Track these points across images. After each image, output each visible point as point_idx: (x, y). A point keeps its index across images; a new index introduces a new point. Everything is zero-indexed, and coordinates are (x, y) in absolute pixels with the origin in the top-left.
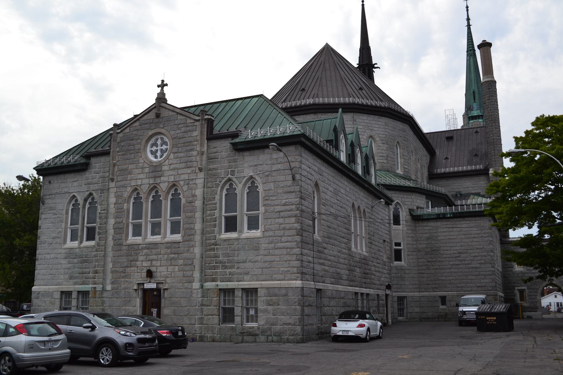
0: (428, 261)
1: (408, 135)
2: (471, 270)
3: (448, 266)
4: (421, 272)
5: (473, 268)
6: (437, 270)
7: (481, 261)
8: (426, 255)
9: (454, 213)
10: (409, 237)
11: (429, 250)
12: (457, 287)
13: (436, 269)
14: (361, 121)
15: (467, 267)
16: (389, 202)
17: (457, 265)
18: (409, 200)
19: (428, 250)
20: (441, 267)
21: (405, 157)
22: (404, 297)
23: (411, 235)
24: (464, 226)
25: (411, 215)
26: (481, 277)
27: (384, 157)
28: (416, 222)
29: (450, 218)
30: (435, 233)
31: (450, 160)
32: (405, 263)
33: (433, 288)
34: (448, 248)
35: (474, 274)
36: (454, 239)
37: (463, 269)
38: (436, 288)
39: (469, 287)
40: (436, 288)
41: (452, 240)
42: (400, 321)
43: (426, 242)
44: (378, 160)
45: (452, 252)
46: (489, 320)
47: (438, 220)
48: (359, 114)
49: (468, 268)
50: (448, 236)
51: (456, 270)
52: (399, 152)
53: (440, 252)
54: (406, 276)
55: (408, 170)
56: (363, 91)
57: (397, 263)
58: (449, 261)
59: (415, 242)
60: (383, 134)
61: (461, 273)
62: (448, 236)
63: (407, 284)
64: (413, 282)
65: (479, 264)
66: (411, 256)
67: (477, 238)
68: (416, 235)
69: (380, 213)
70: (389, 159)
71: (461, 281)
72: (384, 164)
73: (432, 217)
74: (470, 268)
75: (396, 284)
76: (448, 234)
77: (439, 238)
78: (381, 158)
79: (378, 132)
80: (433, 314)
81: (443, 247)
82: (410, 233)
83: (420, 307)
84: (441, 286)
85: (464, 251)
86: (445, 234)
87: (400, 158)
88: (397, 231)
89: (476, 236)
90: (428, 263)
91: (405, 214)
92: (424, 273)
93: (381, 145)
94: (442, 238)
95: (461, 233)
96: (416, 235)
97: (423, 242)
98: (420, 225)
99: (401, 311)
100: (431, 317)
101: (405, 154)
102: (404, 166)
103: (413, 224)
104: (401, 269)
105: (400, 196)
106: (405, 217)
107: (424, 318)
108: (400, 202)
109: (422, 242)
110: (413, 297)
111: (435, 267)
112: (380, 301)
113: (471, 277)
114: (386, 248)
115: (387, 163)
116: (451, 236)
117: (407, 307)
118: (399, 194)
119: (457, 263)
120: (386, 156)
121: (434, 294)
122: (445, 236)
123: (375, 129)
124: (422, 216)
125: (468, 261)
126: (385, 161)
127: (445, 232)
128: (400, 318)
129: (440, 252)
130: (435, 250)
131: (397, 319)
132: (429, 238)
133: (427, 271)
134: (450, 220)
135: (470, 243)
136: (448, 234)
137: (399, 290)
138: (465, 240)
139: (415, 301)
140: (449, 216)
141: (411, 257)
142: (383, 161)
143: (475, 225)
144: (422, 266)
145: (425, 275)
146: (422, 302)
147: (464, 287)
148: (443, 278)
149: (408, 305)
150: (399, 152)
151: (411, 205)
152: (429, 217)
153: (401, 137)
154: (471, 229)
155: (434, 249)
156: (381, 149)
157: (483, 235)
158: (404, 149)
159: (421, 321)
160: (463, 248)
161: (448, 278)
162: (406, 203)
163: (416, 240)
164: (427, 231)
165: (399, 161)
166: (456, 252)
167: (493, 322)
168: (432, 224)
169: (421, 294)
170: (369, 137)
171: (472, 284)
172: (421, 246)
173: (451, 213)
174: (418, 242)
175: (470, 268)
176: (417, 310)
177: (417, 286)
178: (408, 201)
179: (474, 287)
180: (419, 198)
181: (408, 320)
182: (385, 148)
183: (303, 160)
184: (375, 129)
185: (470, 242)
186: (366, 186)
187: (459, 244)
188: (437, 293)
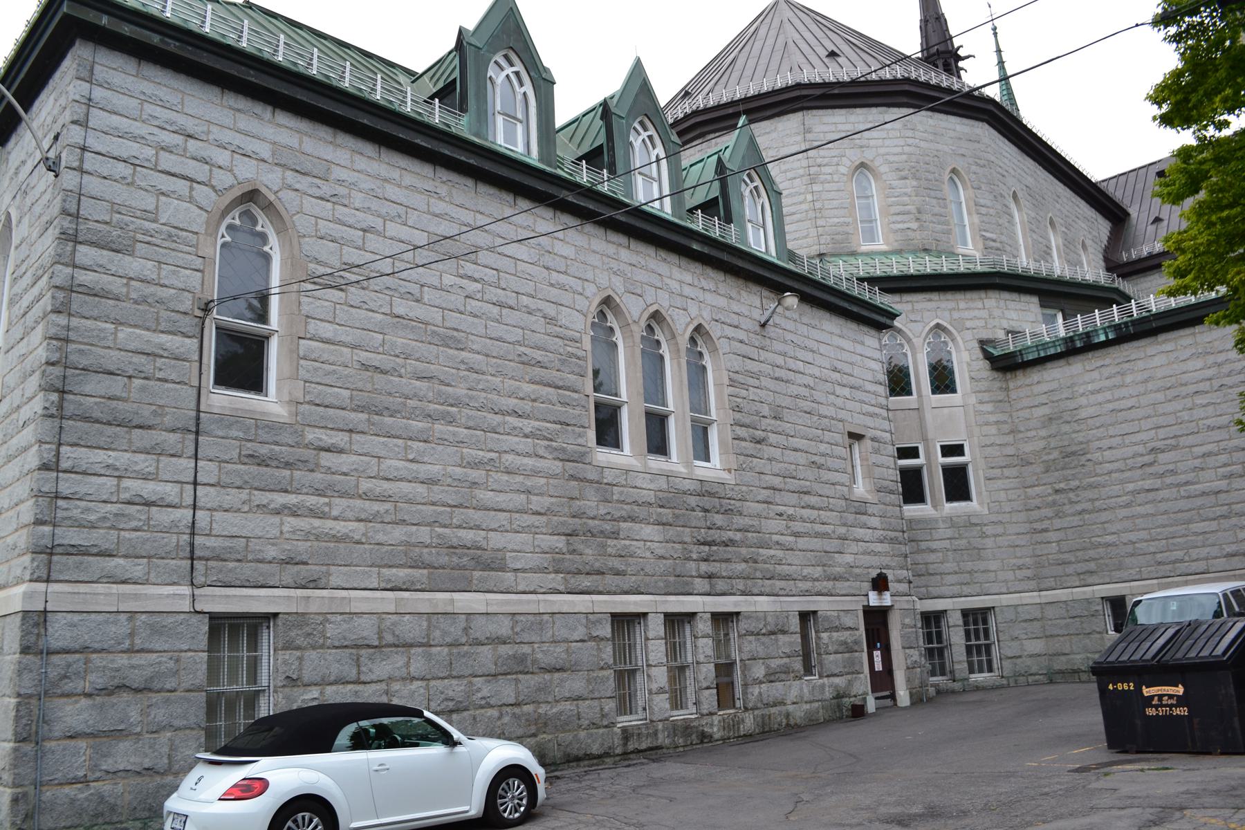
0: (1057, 491)
1: (989, 149)
2: (1199, 502)
3: (1119, 500)
4: (1038, 526)
5: (1203, 494)
6: (1087, 516)
7: (1229, 469)
8: (1047, 471)
9: (1117, 327)
10: (987, 424)
11: (1055, 454)
12: (1159, 563)
13: (1084, 511)
14: (826, 128)
15: (1183, 493)
16: (879, 321)
17: (1148, 491)
18: (976, 313)
19: (1051, 457)
20: (1097, 504)
21: (983, 210)
22: (989, 609)
23: (992, 418)
24: (1157, 361)
25: (988, 356)
26: (1234, 520)
27: (909, 213)
28: (1009, 375)
29: (1107, 344)
30: (1067, 399)
31: (1165, 223)
32: (981, 503)
33: (1079, 574)
34: (1112, 439)
35: (1211, 515)
36: (1130, 409)
37: (1170, 503)
38: (1091, 573)
39: (1197, 560)
40: (1091, 573)
41: (1123, 413)
42: (978, 688)
43: (1043, 433)
44: (892, 226)
45: (1129, 451)
46: (1155, 702)
47: (1071, 359)
48: (821, 112)
49: (1188, 497)
50: (1109, 401)
51: (1149, 509)
52: (963, 199)
53: (1089, 456)
54: (989, 542)
55: (998, 245)
56: (839, 60)
57: (951, 508)
58: (1123, 482)
59: (1010, 439)
60: (901, 154)
61: (1165, 517)
62: (1109, 401)
63: (993, 569)
64: (1014, 561)
65: (1225, 477)
66: (1000, 482)
67: (1207, 392)
68: (1011, 416)
69: (823, 349)
70: (925, 217)
71: (1171, 541)
72: (910, 233)
73: (1052, 351)
74: (1196, 496)
75: (956, 573)
76: (1108, 395)
77: (1083, 414)
78: (899, 218)
79: (882, 151)
80: (1088, 658)
81: (1099, 439)
82: (989, 413)
83: (1047, 637)
84: (1107, 565)
85: (1169, 442)
86: (1100, 397)
87: (969, 213)
88: (946, 411)
89: (1201, 387)
90: (1057, 497)
91: (966, 356)
92: (1045, 530)
93: (895, 183)
94: (1091, 411)
95: (1150, 386)
96: (1011, 416)
97: (1033, 433)
98: (1019, 383)
99: (979, 652)
100: (1083, 668)
101: (982, 201)
102: (984, 233)
103: (997, 384)
104: (970, 523)
105: (943, 305)
106: (969, 365)
107: (1061, 672)
108: (945, 324)
109: (1030, 434)
110: (1016, 606)
111: (1079, 507)
112: (824, 635)
113: (1203, 524)
114: (867, 460)
115: (921, 228)
116: (1117, 400)
117: (998, 641)
118: (940, 300)
119: (1148, 484)
120: (915, 211)
121: (1084, 593)
122: (1100, 404)
123: (872, 143)
124: (1021, 355)
125: (1185, 472)
126: (914, 225)
127: (1099, 391)
128: (978, 677)
129: (1089, 456)
130: (1073, 453)
131: (967, 679)
132: (1050, 419)
133: (1058, 523)
134: (1111, 350)
135: (1185, 416)
136: (1108, 395)
137: (966, 590)
138: (1170, 407)
139: (1026, 621)
140: (1103, 338)
141: (999, 484)
142: (906, 225)
143: (1194, 351)
144: (1039, 508)
145: (1052, 536)
146: (1050, 622)
147: (1182, 561)
148: (1109, 539)
149: (1000, 634)
150: (963, 199)
151: (985, 327)
152: (1042, 354)
153: (963, 155)
154: (1184, 367)
155: (1069, 450)
156: (896, 194)
157: (1227, 381)
158: (979, 188)
159: (1051, 682)
160: (1162, 433)
161: (1126, 537)
162: (969, 324)
163: (1012, 432)
164: (1043, 399)
165: (966, 222)
166: (1140, 449)
167: (1171, 706)
168: (1055, 374)
169: (1046, 596)
170: (857, 168)
171: (1207, 550)
172: (1028, 448)
173: (1109, 327)
174: (1021, 435)
175: (1196, 496)
176: (1036, 646)
177: (1029, 573)
178: (976, 318)
179: (1216, 558)
180: (1012, 305)
181: (1004, 682)
182: (909, 190)
183: (98, 93)
184: (872, 143)
185: (1184, 409)
186: (695, 246)
187: (1146, 424)
188: (1096, 588)
